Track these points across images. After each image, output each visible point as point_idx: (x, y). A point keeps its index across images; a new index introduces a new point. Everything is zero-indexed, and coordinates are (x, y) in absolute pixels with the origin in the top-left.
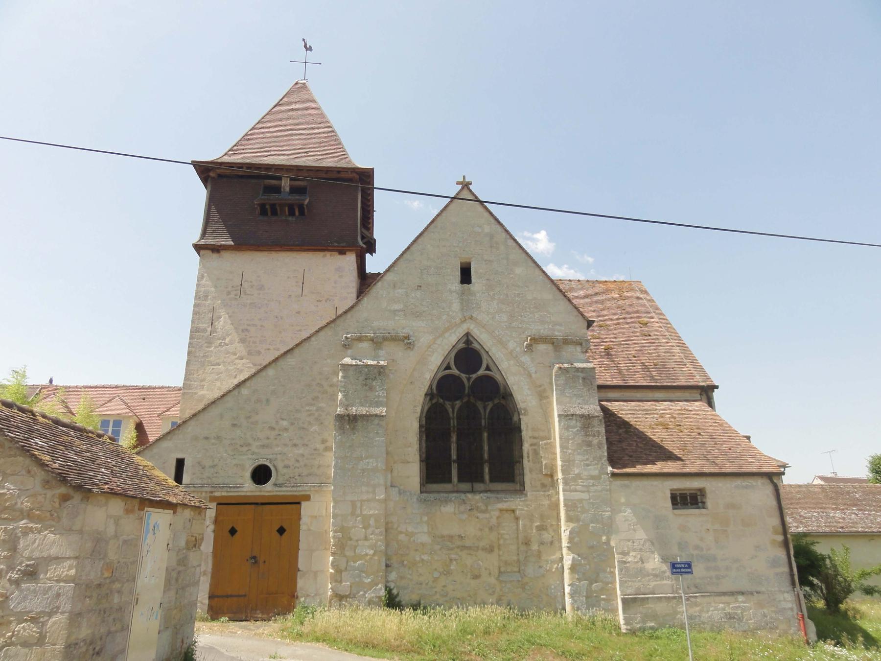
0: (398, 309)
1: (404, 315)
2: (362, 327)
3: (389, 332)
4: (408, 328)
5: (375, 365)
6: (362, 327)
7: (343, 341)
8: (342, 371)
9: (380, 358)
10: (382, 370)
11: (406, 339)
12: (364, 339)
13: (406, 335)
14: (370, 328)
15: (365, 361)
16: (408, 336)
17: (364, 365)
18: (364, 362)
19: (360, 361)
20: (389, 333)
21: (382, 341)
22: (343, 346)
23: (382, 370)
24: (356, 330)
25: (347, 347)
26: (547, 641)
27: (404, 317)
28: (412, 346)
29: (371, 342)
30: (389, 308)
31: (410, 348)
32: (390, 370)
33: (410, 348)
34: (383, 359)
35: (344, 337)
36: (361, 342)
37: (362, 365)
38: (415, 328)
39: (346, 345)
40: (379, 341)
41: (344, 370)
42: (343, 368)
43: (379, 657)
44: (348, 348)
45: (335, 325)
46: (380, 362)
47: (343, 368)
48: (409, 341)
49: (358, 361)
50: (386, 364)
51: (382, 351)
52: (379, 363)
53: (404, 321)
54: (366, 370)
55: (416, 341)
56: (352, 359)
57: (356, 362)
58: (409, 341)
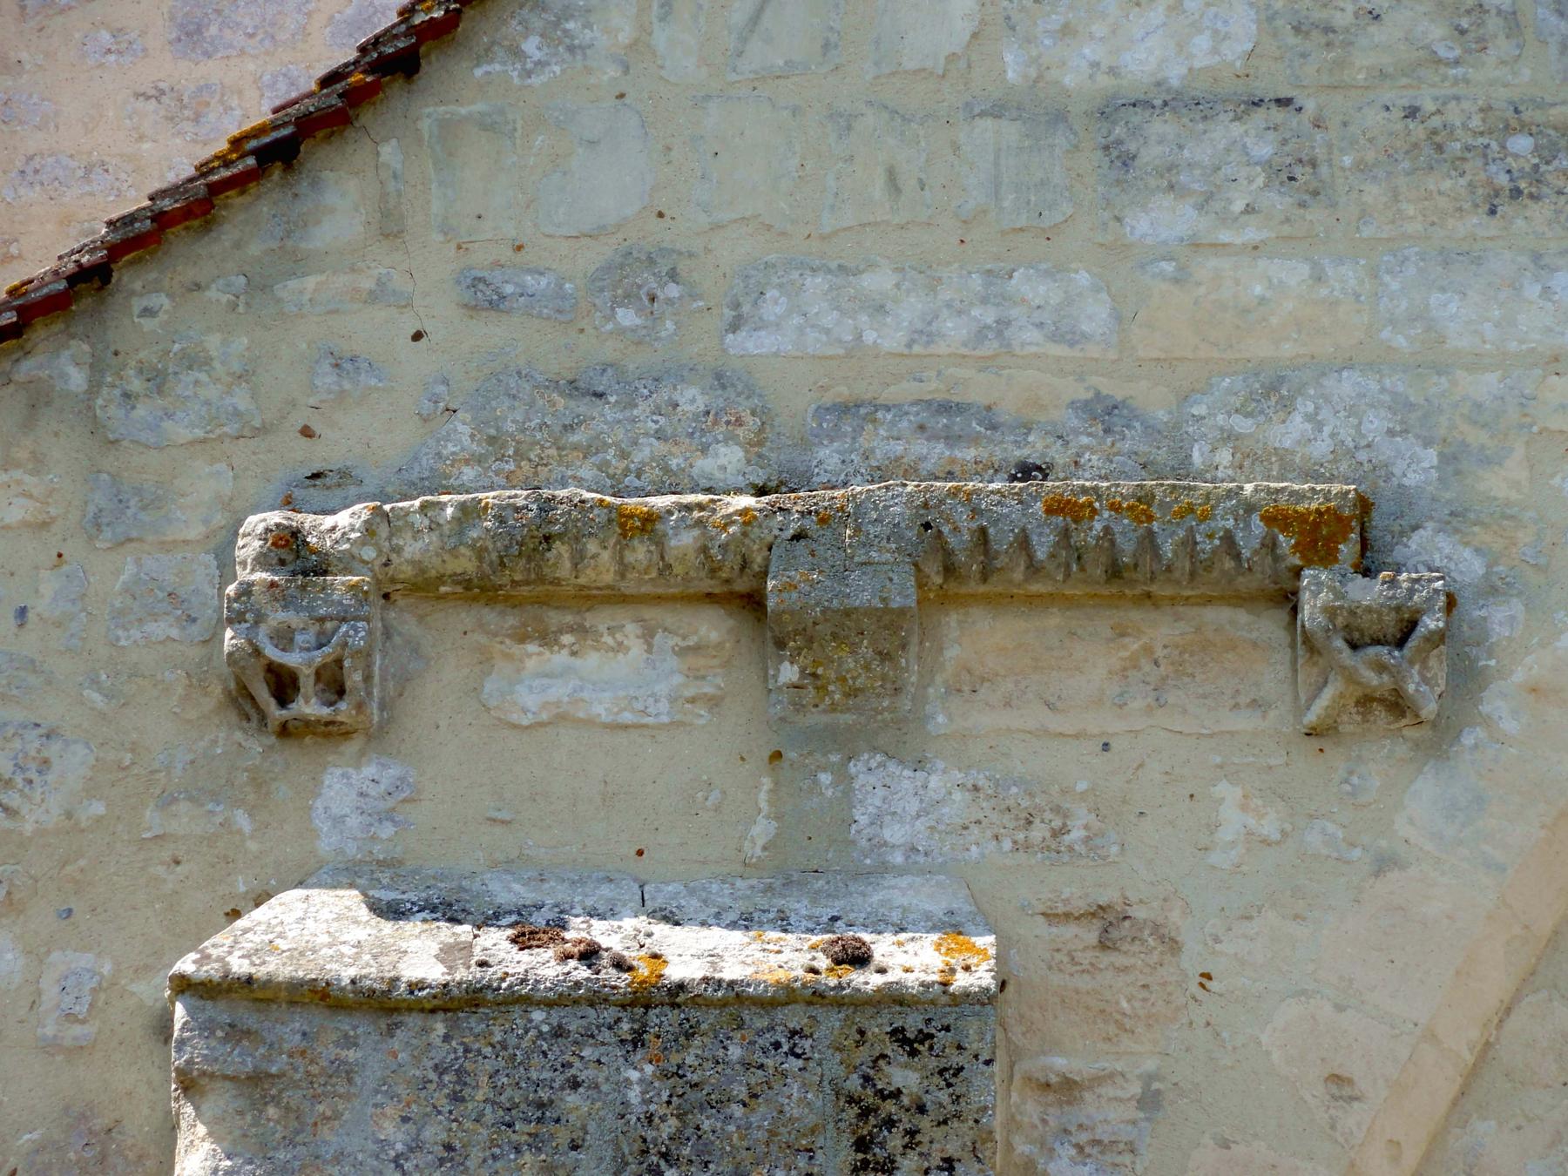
0: (1175, 74)
1: (1284, 175)
2: (573, 388)
3: (1034, 449)
4: (1346, 386)
5: (787, 995)
6: (573, 388)
7: (243, 611)
8: (221, 1099)
9: (898, 893)
10: (904, 1076)
11: (1327, 558)
12: (602, 565)
13: (1313, 495)
14: (692, 399)
15: (612, 935)
16: (1364, 505)
17: (597, 998)
18: (590, 954)
19: (523, 940)
20: (1026, 471)
21: (903, 593)
22: (241, 700)
23: (904, 1076)
24: (462, 434)
25: (309, 706)
26: (1398, 521)
27: (1279, 202)
28: (1438, 666)
29: (711, 627)
30: (1013, 66)
31: (1398, 705)
32: (1066, 1089)
33: (1398, 705)
34: (938, 908)
35: (248, 547)
36: (547, 638)
37: (562, 999)
38: (1485, 386)
39: (283, 685)
40: (863, 592)
41: (257, 1084)
42: (241, 1060)
43: (376, 41)
44: (330, 732)
45: (96, 369)
46: (882, 947)
47: (241, 1060)
48: (1368, 593)
49: (495, 942)
50: (982, 977)
51: (906, 779)
52: (859, 958)
53: (1294, 273)
54: (637, 1075)
55: (1492, 590)
56: (392, 912)
57: (447, 954)
58: (1368, 593)
